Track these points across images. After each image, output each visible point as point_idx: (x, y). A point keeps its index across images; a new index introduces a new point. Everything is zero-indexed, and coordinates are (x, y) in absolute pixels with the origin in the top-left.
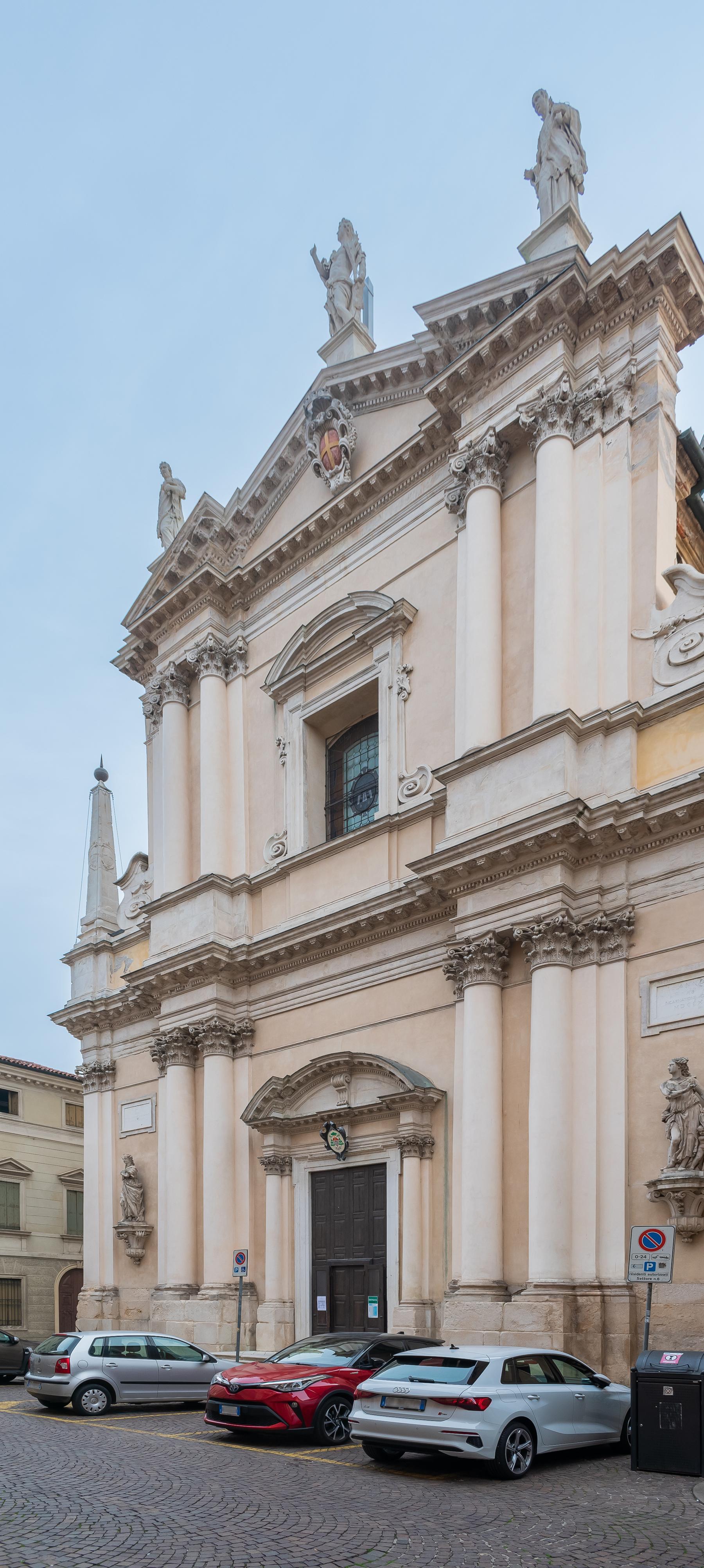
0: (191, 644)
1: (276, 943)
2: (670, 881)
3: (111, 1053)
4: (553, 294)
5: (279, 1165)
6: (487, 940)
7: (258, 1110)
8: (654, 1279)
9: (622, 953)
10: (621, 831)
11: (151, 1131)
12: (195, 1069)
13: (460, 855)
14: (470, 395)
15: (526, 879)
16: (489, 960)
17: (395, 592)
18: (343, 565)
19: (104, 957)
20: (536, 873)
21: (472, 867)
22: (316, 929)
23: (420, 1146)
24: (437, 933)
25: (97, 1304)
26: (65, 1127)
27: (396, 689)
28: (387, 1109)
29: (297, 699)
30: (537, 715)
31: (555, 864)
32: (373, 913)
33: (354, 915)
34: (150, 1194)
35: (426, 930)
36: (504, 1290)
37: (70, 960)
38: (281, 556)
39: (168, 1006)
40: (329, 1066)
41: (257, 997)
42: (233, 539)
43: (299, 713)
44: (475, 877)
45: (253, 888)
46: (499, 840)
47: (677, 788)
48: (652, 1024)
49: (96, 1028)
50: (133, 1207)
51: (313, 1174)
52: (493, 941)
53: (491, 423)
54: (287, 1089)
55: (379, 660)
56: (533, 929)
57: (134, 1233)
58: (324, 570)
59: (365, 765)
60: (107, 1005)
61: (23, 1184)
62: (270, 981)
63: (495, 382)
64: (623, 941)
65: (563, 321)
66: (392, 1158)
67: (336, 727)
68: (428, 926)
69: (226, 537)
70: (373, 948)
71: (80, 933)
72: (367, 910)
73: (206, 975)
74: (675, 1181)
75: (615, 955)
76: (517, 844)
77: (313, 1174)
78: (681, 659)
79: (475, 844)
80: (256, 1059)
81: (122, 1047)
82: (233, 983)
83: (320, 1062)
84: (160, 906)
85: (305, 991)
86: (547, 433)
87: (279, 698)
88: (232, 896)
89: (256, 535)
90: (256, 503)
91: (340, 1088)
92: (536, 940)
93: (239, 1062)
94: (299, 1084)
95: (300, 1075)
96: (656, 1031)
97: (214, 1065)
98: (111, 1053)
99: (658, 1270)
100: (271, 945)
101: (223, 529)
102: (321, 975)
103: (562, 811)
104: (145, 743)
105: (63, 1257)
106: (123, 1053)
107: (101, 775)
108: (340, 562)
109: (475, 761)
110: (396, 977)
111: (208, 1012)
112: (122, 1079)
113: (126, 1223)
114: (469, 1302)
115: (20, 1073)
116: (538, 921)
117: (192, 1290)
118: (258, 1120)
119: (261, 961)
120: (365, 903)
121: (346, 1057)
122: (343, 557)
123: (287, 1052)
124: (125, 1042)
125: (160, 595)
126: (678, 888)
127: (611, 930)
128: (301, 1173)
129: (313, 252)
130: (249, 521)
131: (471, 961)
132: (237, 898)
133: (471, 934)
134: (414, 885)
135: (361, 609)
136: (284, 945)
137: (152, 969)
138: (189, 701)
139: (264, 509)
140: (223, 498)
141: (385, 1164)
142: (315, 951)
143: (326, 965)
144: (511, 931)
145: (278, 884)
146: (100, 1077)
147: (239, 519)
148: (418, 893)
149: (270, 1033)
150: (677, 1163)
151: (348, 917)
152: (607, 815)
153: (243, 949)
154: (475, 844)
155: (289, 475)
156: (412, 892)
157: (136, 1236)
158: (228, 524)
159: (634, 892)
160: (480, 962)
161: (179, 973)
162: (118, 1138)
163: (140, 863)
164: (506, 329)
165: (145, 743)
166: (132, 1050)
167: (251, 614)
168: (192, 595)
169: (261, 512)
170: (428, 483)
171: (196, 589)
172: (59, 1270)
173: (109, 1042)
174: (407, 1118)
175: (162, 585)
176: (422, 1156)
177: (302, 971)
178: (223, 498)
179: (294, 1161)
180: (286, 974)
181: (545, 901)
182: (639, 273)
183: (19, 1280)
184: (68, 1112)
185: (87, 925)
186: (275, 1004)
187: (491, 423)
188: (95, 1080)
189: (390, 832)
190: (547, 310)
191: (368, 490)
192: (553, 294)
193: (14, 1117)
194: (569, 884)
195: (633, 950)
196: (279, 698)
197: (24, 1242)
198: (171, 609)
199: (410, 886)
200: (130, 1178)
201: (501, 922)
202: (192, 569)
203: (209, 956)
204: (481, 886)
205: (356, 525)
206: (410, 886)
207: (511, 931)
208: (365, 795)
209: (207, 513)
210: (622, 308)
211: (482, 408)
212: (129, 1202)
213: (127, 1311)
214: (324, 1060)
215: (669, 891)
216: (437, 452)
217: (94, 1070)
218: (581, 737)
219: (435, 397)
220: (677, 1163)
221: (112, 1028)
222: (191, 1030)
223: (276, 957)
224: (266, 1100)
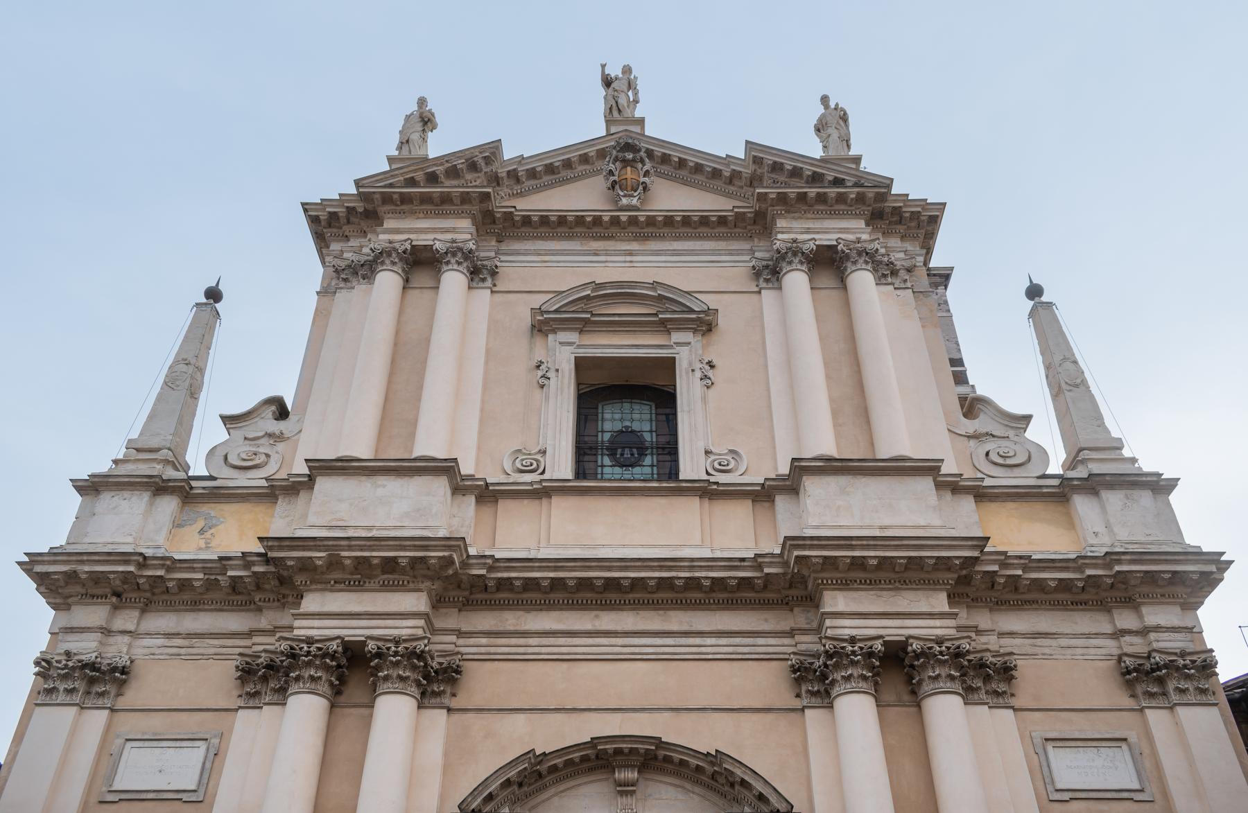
0: (449, 236)
1: (540, 569)
2: (1039, 642)
3: (130, 646)
4: (870, 193)
6: (334, 646)
10: (170, 584)
13: (851, 547)
14: (788, 212)
15: (910, 595)
16: (327, 668)
17: (711, 301)
18: (628, 258)
19: (168, 505)
20: (919, 593)
21: (858, 563)
22: (609, 569)
24: (766, 620)
30: (417, 453)
31: (941, 590)
32: (697, 574)
33: (670, 568)
35: (750, 613)
37: (91, 487)
38: (562, 221)
39: (312, 602)
40: (618, 752)
41: (480, 628)
42: (498, 184)
44: (853, 575)
45: (487, 495)
46: (897, 547)
47: (1053, 561)
48: (113, 788)
49: (114, 599)
52: (340, 649)
53: (412, 236)
56: (388, 649)
59: (628, 424)
60: (1025, 569)
62: (497, 613)
63: (809, 216)
64: (112, 689)
65: (867, 210)
67: (598, 378)
68: (753, 609)
69: (495, 180)
70: (672, 613)
71: (121, 456)
72: (691, 568)
73: (415, 577)
75: (100, 702)
76: (916, 557)
79: (872, 543)
80: (456, 717)
82: (439, 601)
83: (606, 743)
84: (343, 468)
85: (562, 641)
86: (786, 268)
88: (453, 494)
89: (520, 195)
90: (532, 174)
92: (391, 662)
93: (428, 713)
94: (554, 769)
95: (560, 757)
96: (1066, 796)
97: (394, 711)
98: (130, 646)
100: (532, 569)
101: (496, 173)
102: (588, 626)
103: (970, 543)
104: (318, 293)
106: (158, 651)
107: (214, 295)
108: (626, 255)
109: (343, 467)
110: (710, 657)
111: (405, 628)
112: (133, 696)
116: (397, 641)
119: (504, 584)
120: (692, 560)
121: (651, 744)
123: (521, 717)
124: (169, 635)
125: (412, 182)
126: (1047, 651)
127: (104, 673)
129: (603, 66)
130: (518, 181)
131: (309, 664)
132: (460, 498)
134: (766, 560)
135: (661, 297)
136: (552, 575)
137: (331, 543)
139: (536, 182)
140: (508, 153)
142: (589, 595)
143: (597, 616)
144: (364, 644)
145: (526, 502)
146: (92, 681)
147: (513, 175)
149: (482, 683)
151: (661, 568)
152: (994, 562)
153: (489, 561)
154: (872, 543)
155: (570, 174)
156: (759, 567)
158: (502, 172)
160: (317, 668)
161: (375, 561)
162: (94, 799)
163: (273, 408)
164: (812, 192)
165: (318, 293)
166: (183, 651)
167: (503, 247)
168: (457, 201)
169: (532, 182)
171: (465, 199)
173: (131, 627)
175: (419, 176)
177: (555, 614)
178: (508, 153)
180: (528, 611)
181: (938, 623)
182: (915, 216)
185: (138, 450)
186: (503, 646)
187: (412, 236)
188: (80, 685)
189: (701, 497)
190: (861, 199)
192: (870, 193)
195: (121, 699)
198: (426, 199)
199: (760, 560)
201: (354, 631)
202: (455, 182)
203: (446, 554)
204: (856, 586)
205: (646, 238)
206: (760, 560)
207: (364, 644)
208: (627, 451)
209: (493, 154)
210: (899, 227)
211: (796, 225)
214: (612, 742)
215: (1037, 650)
216: (737, 230)
217: (84, 666)
218: (939, 486)
221: (146, 608)
222: (371, 646)
223: (531, 585)
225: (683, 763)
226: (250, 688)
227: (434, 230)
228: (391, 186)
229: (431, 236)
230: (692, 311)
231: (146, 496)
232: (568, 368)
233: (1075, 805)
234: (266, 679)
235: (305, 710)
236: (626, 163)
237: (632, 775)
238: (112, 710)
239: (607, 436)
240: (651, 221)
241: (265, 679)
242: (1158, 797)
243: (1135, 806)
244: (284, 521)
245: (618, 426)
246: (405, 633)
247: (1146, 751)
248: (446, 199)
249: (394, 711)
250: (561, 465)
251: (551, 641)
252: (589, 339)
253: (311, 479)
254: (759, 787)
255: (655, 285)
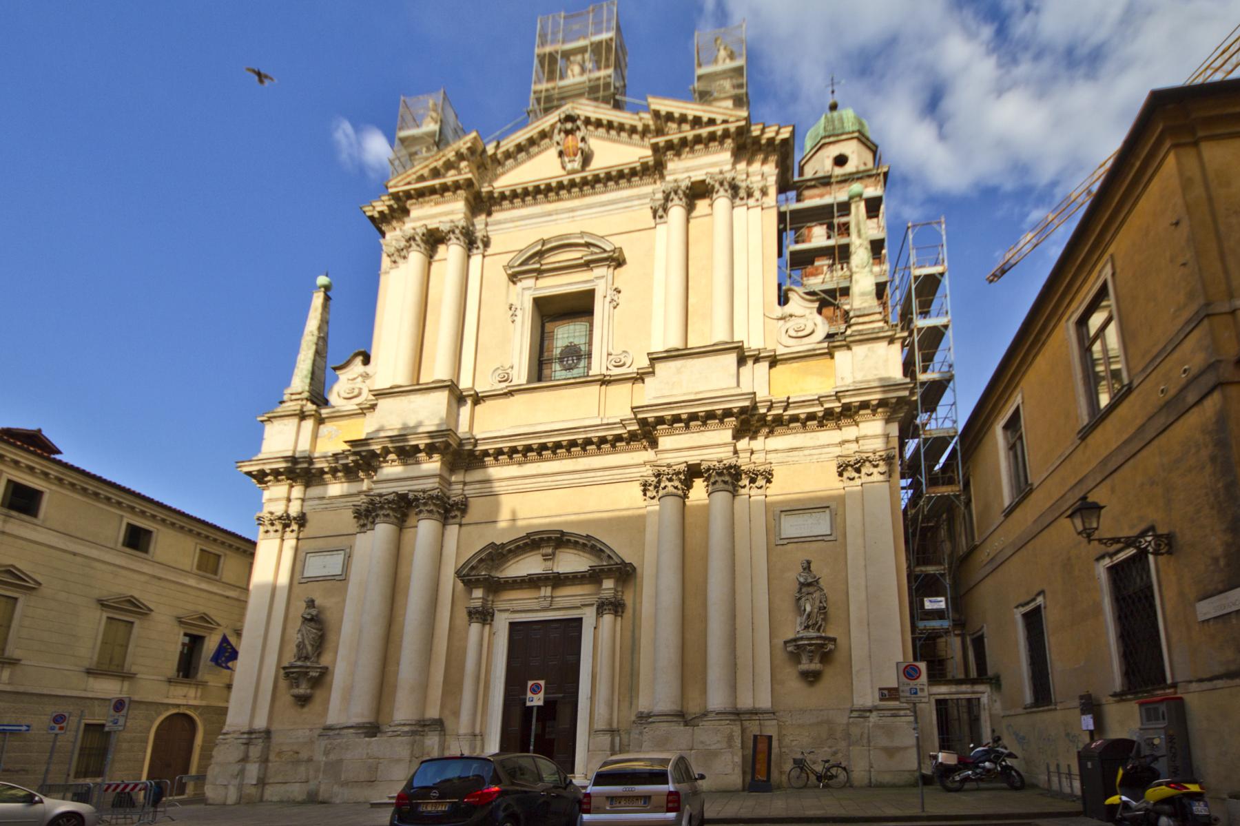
5: (483, 615)
6: (391, 497)
7: (473, 568)
8: (917, 700)
9: (457, 520)
11: (342, 579)
12: (734, 496)
17: (617, 242)
18: (571, 214)
22: (540, 438)
23: (615, 607)
25: (242, 747)
26: (195, 570)
27: (608, 299)
28: (593, 577)
29: (529, 282)
34: (331, 637)
36: (681, 717)
40: (542, 539)
43: (531, 292)
45: (639, 378)
50: (309, 648)
51: (511, 624)
54: (498, 554)
55: (597, 278)
57: (306, 673)
58: (557, 212)
61: (137, 623)
64: (458, 513)
66: (589, 616)
74: (812, 639)
77: (511, 624)
78: (794, 334)
81: (317, 502)
85: (519, 482)
87: (514, 278)
91: (547, 558)
94: (510, 551)
97: (425, 528)
99: (920, 694)
105: (166, 701)
113: (299, 663)
114: (664, 727)
115: (161, 514)
116: (424, 491)
117: (372, 730)
118: (468, 577)
122: (572, 210)
128: (502, 623)
133: (384, 491)
138: (431, 257)
141: (581, 619)
148: (629, 428)
150: (807, 627)
157: (305, 676)
159: (769, 456)
170: (648, 189)
171: (457, 186)
172: (159, 714)
174: (608, 584)
176: (616, 613)
179: (497, 613)
183: (938, 702)
184: (201, 558)
190: (726, 134)
191: (585, 182)
193: (143, 555)
194: (446, 475)
196: (514, 278)
197: (126, 684)
198: (432, 191)
200: (312, 620)
207: (699, 465)
212: (307, 642)
213: (280, 753)
219: (655, 148)
220: (807, 627)
222: (411, 496)
224: (481, 560)
225: (576, 542)
226: (362, 522)
227: (441, 214)
228: (409, 183)
229: (437, 220)
230: (605, 251)
231: (630, 385)
232: (528, 306)
233: (790, 546)
234: (367, 514)
235: (383, 530)
236: (568, 132)
237: (550, 551)
238: (461, 525)
239: (559, 351)
240: (597, 179)
241: (367, 517)
242: (840, 539)
243: (824, 544)
244: (651, 393)
245: (566, 343)
246: (430, 486)
247: (840, 513)
248: (445, 188)
249: (425, 528)
250: (520, 376)
251: (514, 482)
252: (543, 282)
253: (652, 365)
254: (608, 552)
255: (583, 234)
